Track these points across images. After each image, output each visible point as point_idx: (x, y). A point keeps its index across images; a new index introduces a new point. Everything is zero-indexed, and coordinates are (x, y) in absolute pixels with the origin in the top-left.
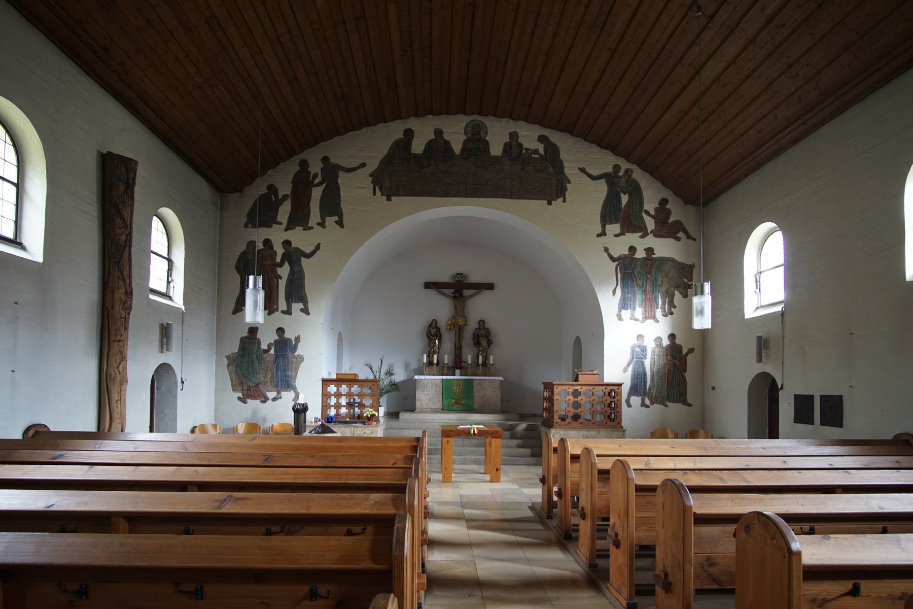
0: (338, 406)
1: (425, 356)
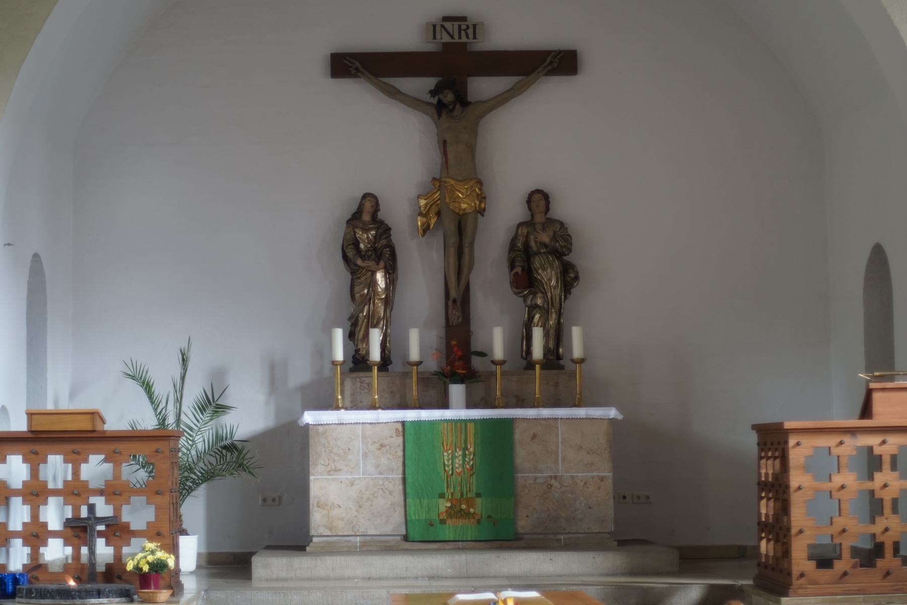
1: (339, 335)
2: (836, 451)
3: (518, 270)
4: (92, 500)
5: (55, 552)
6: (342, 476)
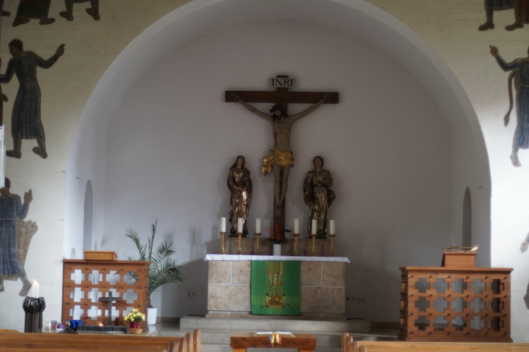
0: (86, 304)
1: (224, 220)
2: (447, 280)
3: (307, 193)
4: (111, 290)
5: (94, 313)
6: (223, 284)
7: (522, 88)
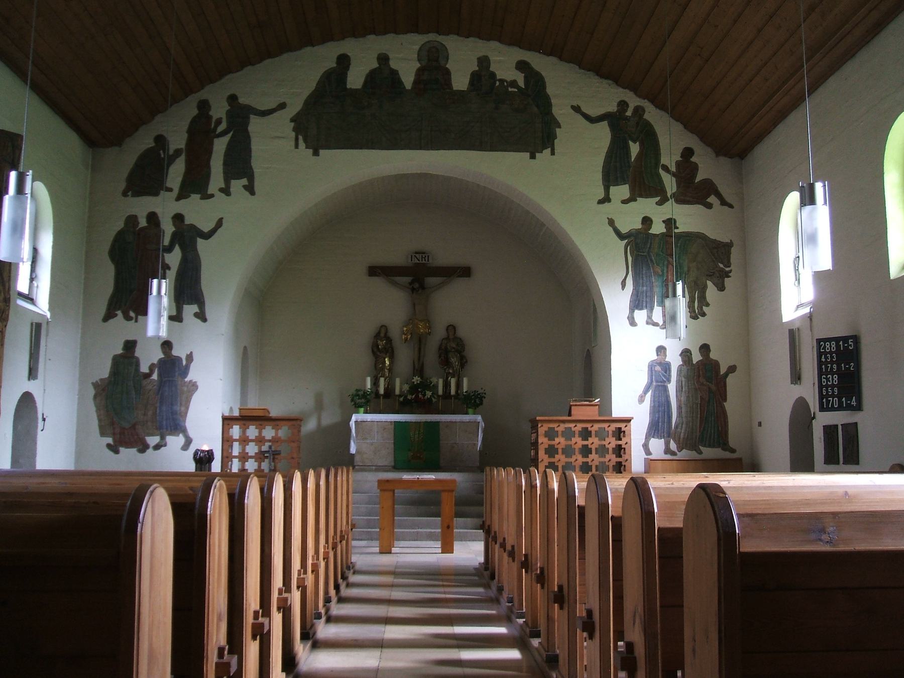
7: (637, 256)
